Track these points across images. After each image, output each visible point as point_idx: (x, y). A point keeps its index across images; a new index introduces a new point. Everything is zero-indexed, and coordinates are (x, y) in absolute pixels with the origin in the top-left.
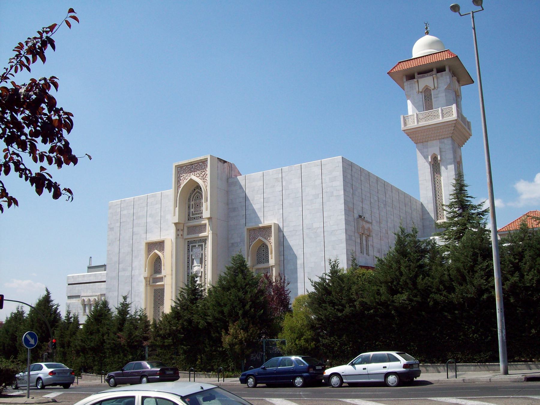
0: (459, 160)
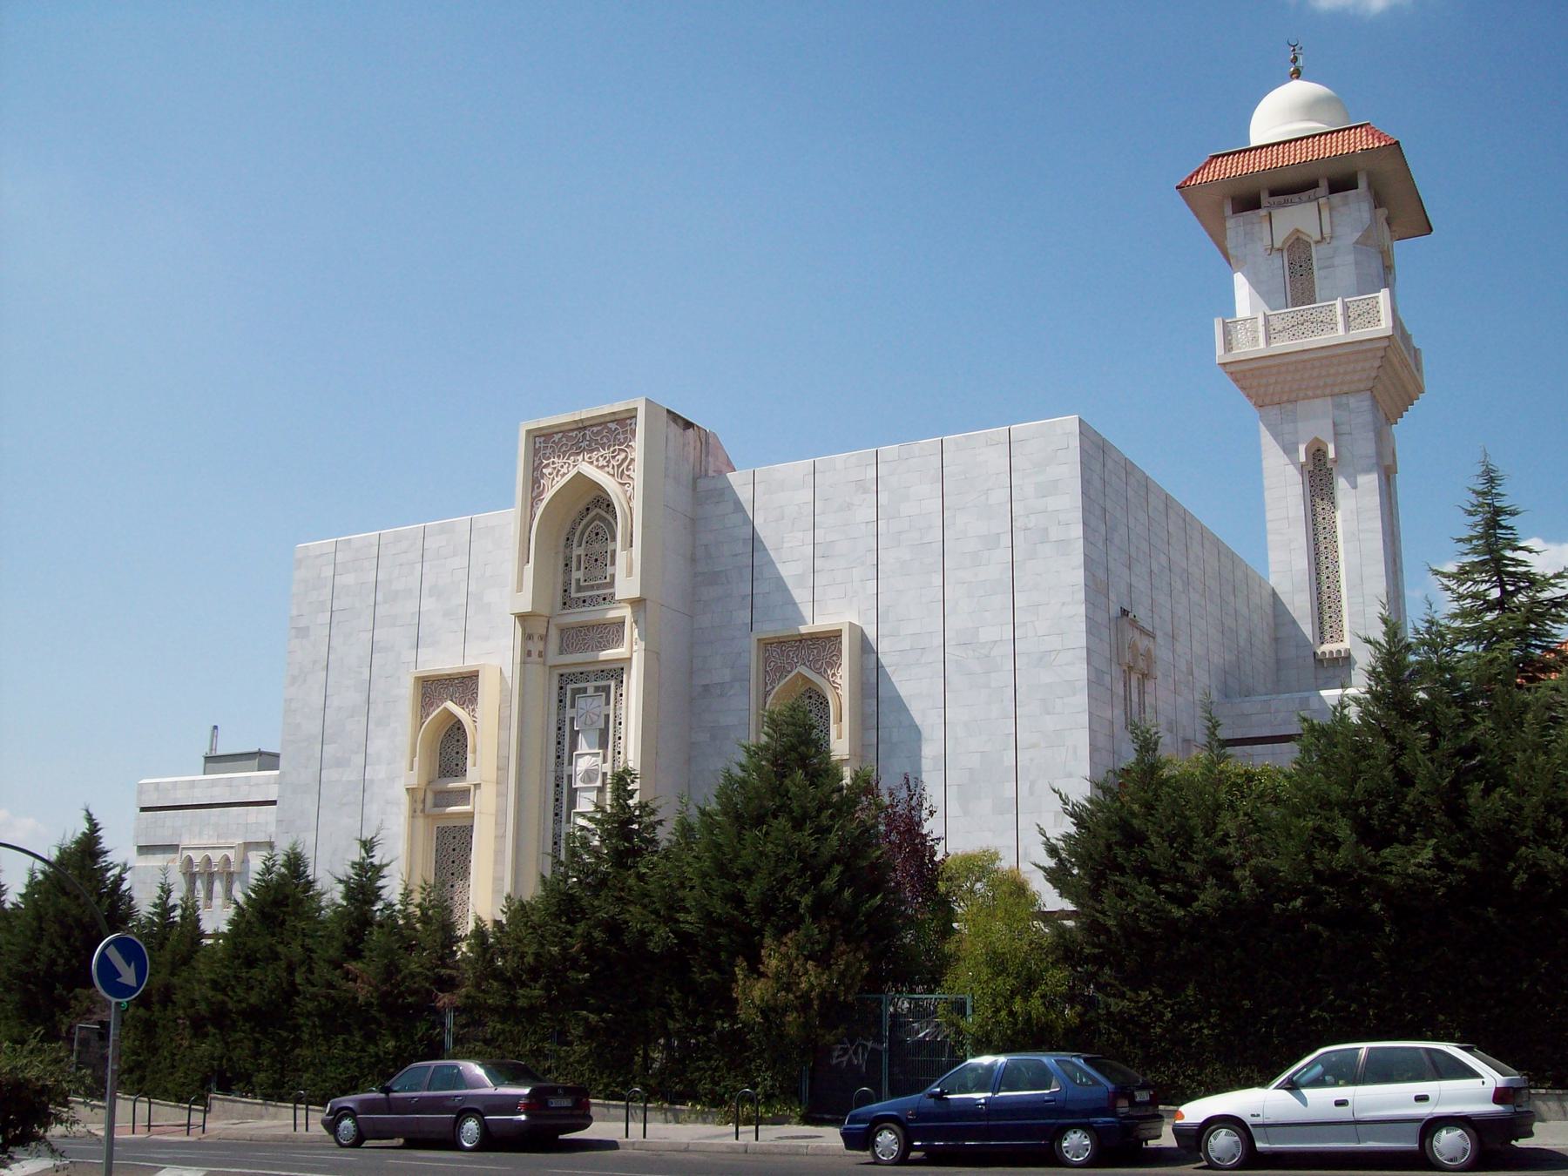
0: (1388, 462)
